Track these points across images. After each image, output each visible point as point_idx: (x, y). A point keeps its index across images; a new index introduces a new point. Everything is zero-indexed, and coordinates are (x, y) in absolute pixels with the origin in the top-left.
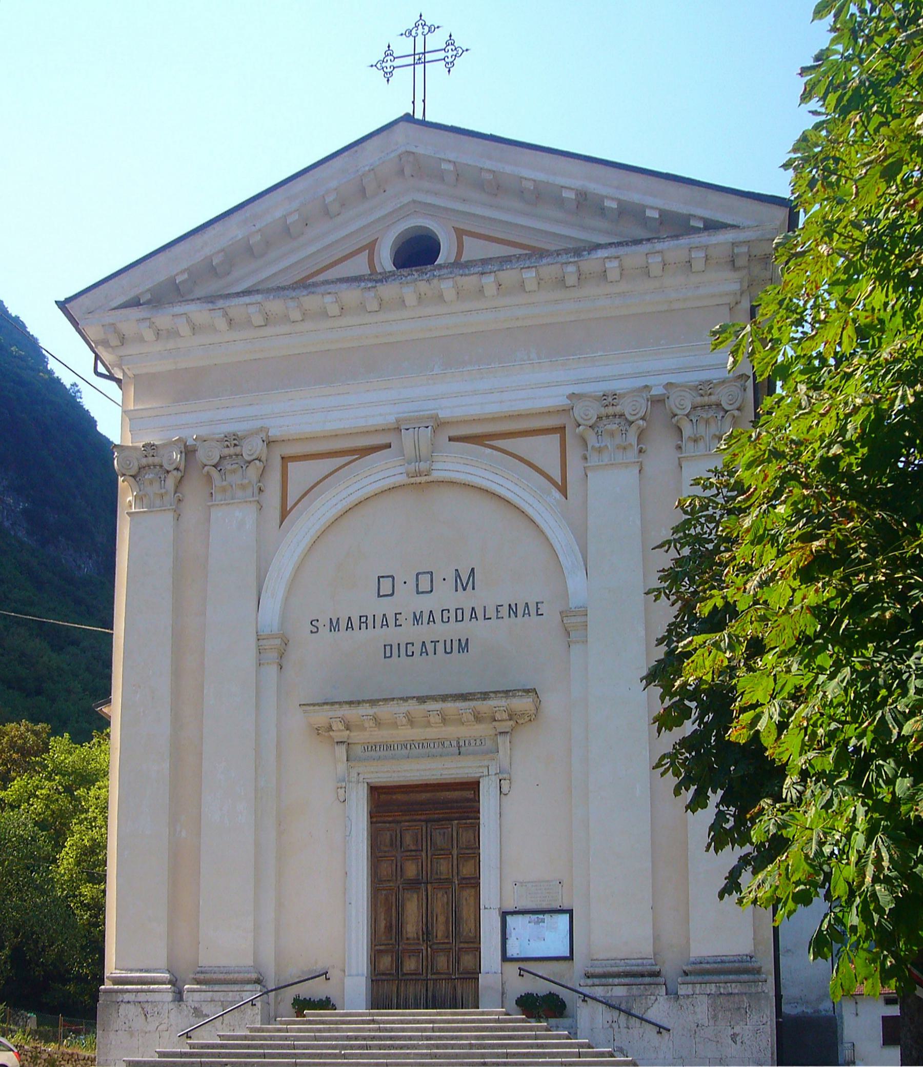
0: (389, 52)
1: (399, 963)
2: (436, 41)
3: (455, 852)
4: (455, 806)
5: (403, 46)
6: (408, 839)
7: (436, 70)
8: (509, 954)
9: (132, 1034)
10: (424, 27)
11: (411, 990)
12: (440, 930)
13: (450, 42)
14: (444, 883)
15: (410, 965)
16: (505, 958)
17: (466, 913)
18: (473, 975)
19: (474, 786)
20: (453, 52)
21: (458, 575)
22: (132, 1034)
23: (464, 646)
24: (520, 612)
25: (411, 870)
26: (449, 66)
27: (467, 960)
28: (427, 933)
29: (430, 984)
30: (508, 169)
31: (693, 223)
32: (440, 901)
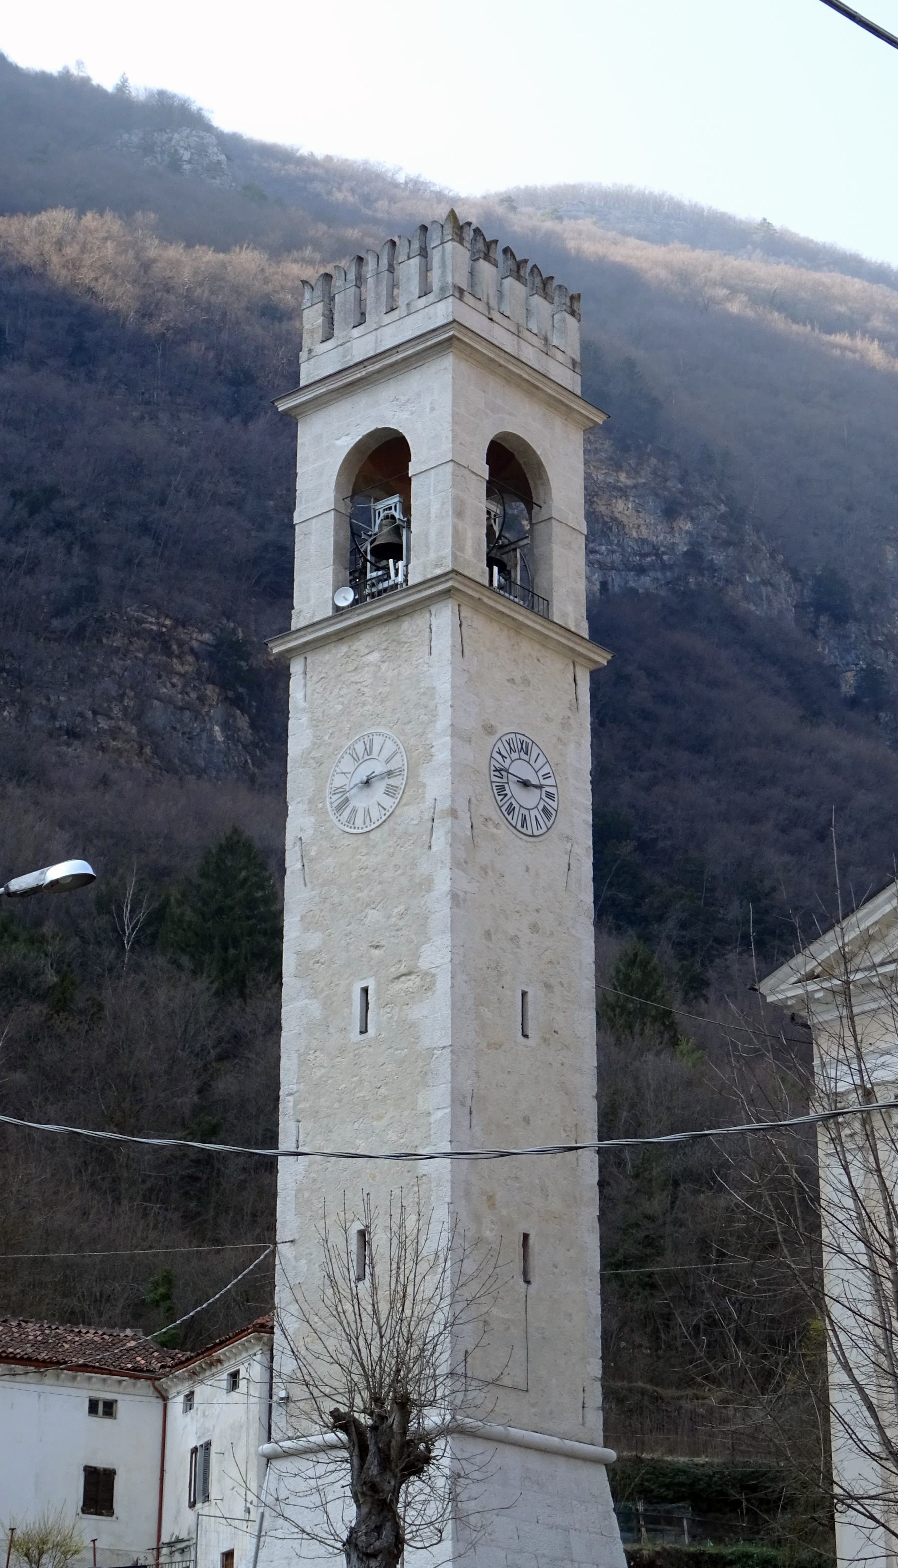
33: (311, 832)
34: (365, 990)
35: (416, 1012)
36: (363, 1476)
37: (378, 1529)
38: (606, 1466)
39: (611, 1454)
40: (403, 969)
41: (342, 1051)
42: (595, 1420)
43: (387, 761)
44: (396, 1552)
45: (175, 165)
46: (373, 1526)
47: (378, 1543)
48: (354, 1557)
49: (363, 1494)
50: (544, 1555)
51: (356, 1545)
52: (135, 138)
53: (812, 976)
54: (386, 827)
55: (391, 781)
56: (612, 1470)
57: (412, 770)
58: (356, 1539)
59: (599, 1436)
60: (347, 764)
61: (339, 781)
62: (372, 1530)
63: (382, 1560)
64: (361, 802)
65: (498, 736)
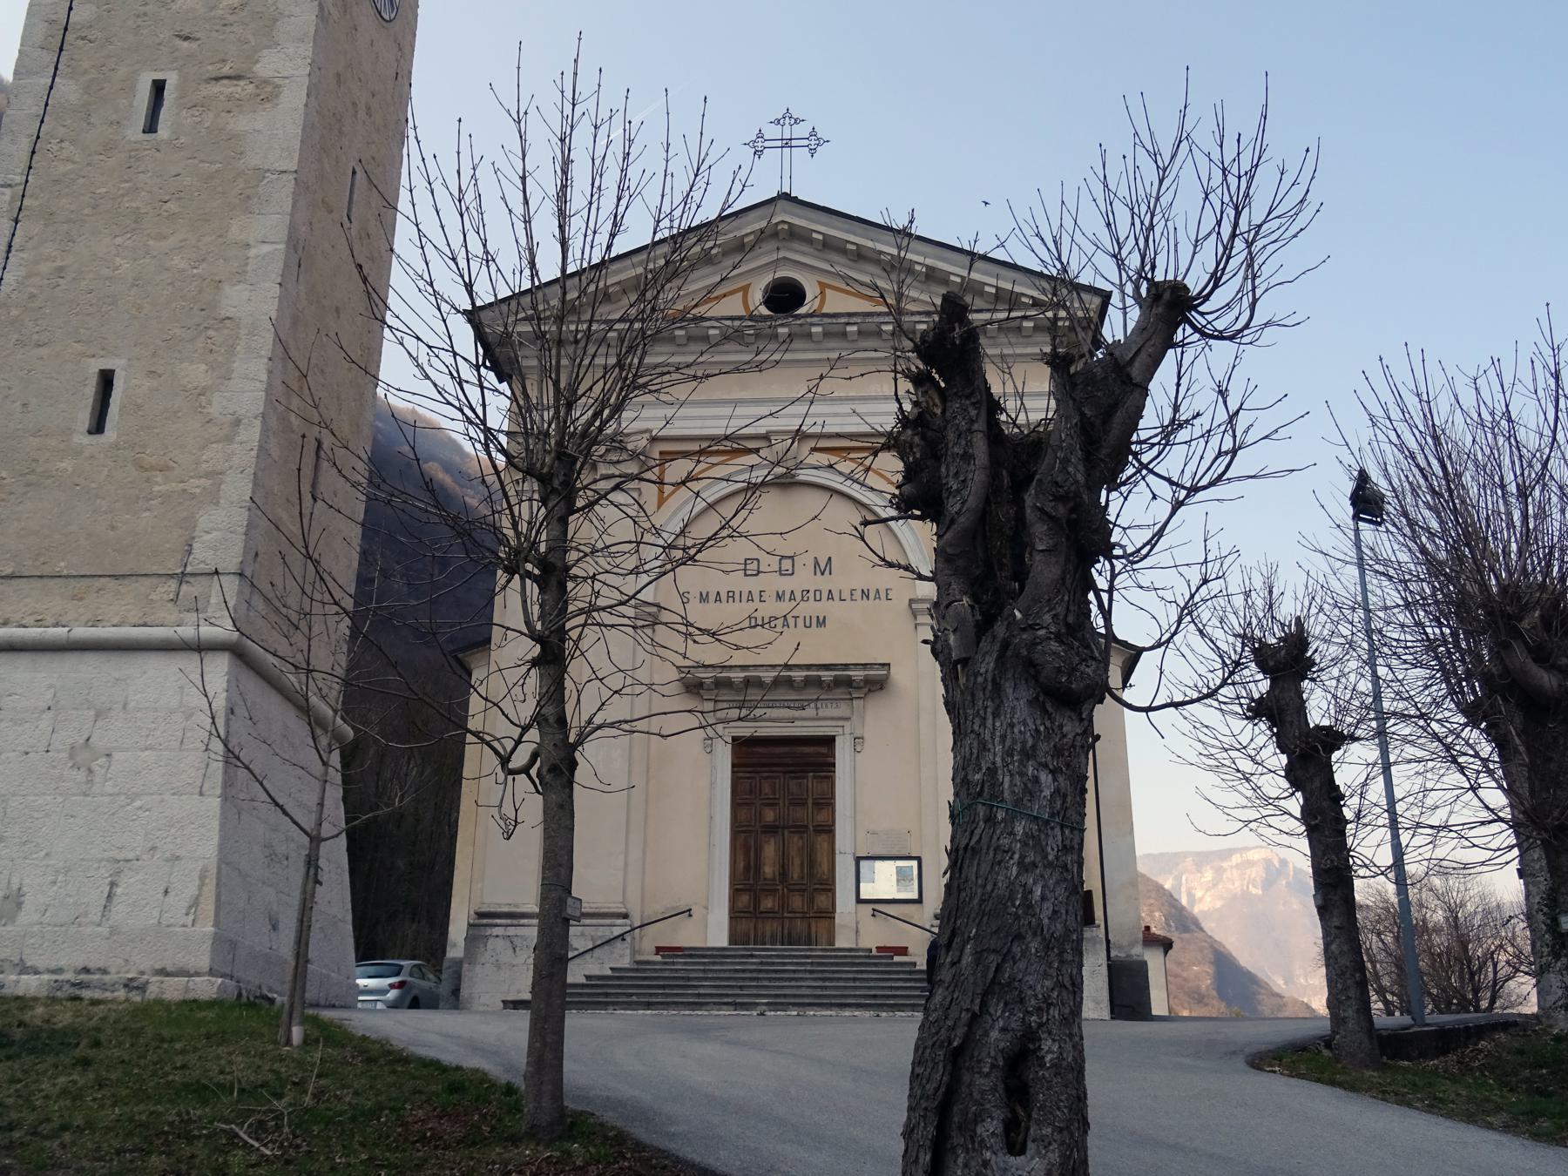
0: (760, 135)
1: (757, 902)
2: (801, 131)
3: (810, 801)
4: (814, 757)
5: (773, 132)
6: (766, 788)
7: (801, 154)
9: (499, 967)
10: (788, 119)
11: (769, 928)
12: (795, 873)
13: (813, 133)
14: (801, 829)
15: (768, 903)
16: (859, 901)
17: (822, 857)
18: (828, 914)
19: (829, 741)
20: (815, 142)
21: (817, 563)
22: (499, 967)
23: (821, 622)
24: (872, 596)
25: (770, 816)
26: (813, 152)
27: (821, 901)
28: (784, 873)
30: (870, 244)
31: (1024, 300)
32: (795, 843)
34: (159, 87)
35: (240, 123)
40: (226, 70)
41: (109, 148)
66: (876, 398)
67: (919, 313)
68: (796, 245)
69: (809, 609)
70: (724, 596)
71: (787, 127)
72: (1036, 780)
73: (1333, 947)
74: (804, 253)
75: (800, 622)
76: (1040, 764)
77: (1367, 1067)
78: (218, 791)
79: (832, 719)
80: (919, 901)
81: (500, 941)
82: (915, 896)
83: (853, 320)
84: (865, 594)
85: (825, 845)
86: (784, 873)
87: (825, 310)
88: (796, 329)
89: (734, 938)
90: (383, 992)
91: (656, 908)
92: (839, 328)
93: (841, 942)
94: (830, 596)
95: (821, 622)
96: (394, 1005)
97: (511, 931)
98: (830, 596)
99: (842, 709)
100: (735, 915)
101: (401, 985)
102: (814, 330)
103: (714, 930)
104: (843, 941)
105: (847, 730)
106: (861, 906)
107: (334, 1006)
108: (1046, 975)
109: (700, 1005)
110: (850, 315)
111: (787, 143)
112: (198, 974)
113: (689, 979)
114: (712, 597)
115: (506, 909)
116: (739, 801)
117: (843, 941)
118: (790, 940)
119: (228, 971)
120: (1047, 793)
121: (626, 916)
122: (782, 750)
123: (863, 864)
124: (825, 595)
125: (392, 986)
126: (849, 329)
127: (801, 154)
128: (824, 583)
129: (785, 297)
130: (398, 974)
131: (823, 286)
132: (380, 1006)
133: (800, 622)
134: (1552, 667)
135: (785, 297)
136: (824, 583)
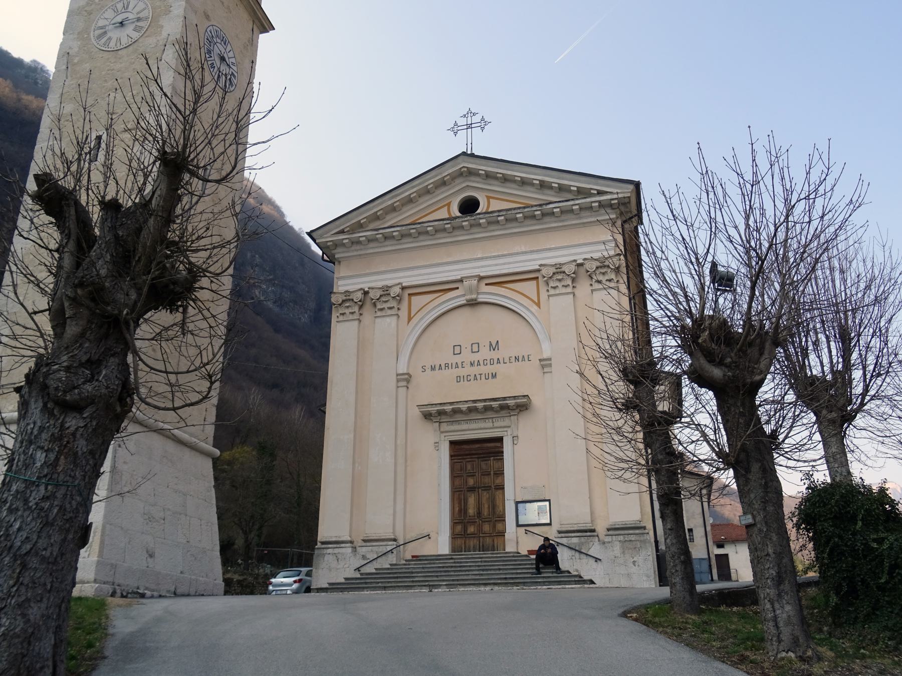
0: (456, 124)
4: (491, 449)
6: (469, 467)
7: (476, 131)
8: (520, 523)
10: (471, 113)
11: (472, 542)
12: (485, 512)
14: (487, 488)
15: (471, 529)
16: (518, 525)
17: (498, 502)
18: (502, 534)
19: (500, 440)
20: (484, 124)
21: (491, 344)
25: (471, 482)
27: (499, 526)
28: (479, 513)
29: (481, 539)
30: (509, 173)
32: (485, 495)
33: (76, 50)
36: (80, 274)
37: (94, 365)
38: (213, 459)
39: (217, 452)
42: (210, 430)
43: (138, 13)
44: (119, 409)
45: (36, 83)
46: (84, 358)
47: (88, 387)
48: (35, 407)
49: (74, 300)
50: (169, 510)
51: (45, 387)
52: (23, 72)
53: (342, 232)
54: (131, 48)
55: (138, 24)
56: (216, 461)
57: (155, 19)
58: (46, 375)
59: (211, 440)
60: (109, 14)
61: (101, 23)
62: (82, 365)
63: (92, 418)
64: (114, 34)
65: (211, 23)
66: (517, 254)
67: (536, 206)
68: (473, 178)
69: (489, 369)
70: (443, 367)
71: (469, 118)
72: (32, 457)
73: (668, 541)
74: (478, 182)
75: (483, 376)
76: (39, 447)
77: (688, 612)
78: (106, 487)
79: (501, 427)
80: (550, 524)
81: (331, 556)
82: (548, 522)
83: (501, 214)
84: (517, 359)
85: (501, 496)
86: (479, 513)
87: (490, 210)
88: (473, 222)
89: (454, 549)
90: (290, 585)
91: (411, 535)
92: (495, 219)
93: (509, 549)
94: (498, 361)
95: (494, 376)
96: (296, 592)
97: (336, 551)
98: (498, 361)
99: (506, 422)
100: (454, 536)
101: (300, 581)
102: (481, 221)
103: (442, 545)
104: (510, 548)
105: (509, 433)
106: (519, 529)
107: (203, 595)
108: (11, 577)
109: (411, 587)
110: (499, 211)
111: (469, 126)
112: (88, 582)
113: (412, 573)
114: (437, 367)
115: (334, 539)
116: (454, 476)
117: (510, 548)
118: (483, 548)
119: (111, 580)
120: (38, 464)
121: (395, 540)
122: (477, 446)
123: (519, 505)
124: (496, 361)
125: (295, 582)
126: (499, 218)
127: (476, 131)
128: (495, 355)
129: (469, 206)
130: (298, 575)
131: (488, 198)
132: (289, 592)
133: (483, 376)
134: (720, 364)
135: (469, 206)
136: (495, 355)
